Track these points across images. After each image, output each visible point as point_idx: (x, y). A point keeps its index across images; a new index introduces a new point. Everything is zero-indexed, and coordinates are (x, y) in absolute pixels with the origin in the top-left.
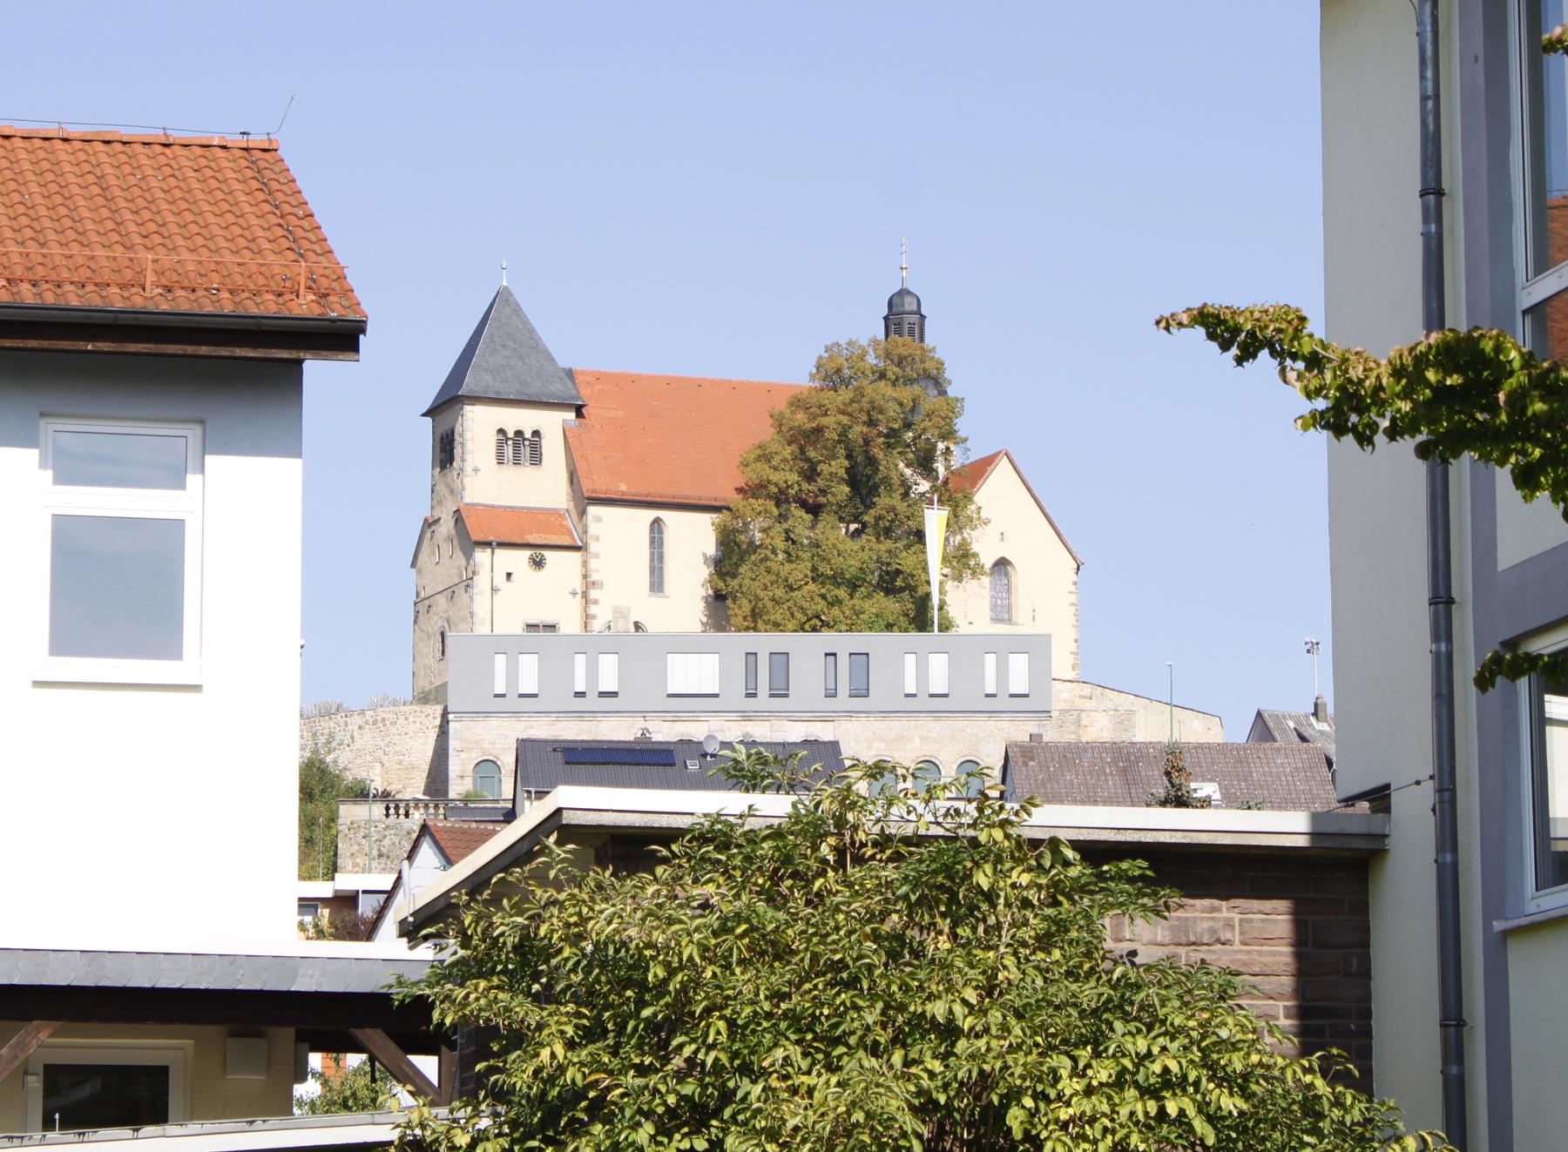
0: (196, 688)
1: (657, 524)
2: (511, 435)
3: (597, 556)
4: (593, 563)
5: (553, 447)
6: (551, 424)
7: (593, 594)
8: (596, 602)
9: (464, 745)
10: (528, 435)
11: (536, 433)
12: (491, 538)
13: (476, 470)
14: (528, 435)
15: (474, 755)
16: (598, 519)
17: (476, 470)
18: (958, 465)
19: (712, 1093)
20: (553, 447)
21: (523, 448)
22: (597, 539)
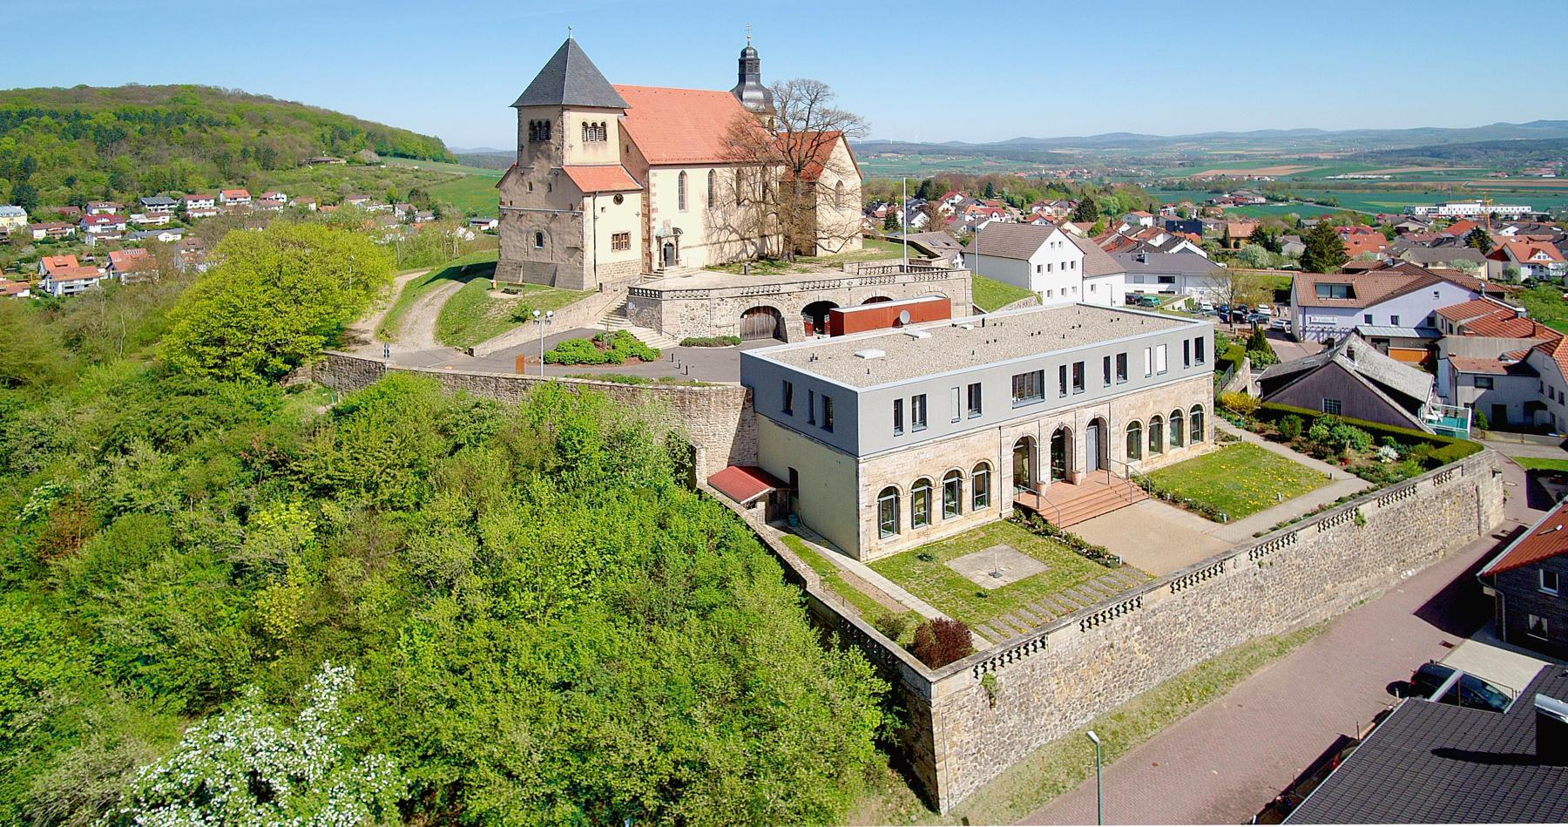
0: (1442, 752)
1: (682, 174)
2: (590, 125)
3: (655, 194)
4: (652, 199)
5: (612, 130)
6: (611, 120)
7: (653, 215)
8: (654, 220)
9: (871, 480)
10: (599, 125)
11: (603, 124)
12: (918, 329)
13: (571, 146)
14: (599, 125)
15: (879, 486)
16: (655, 175)
17: (571, 146)
18: (1495, 525)
19: (1539, 624)
20: (612, 130)
21: (596, 132)
22: (654, 185)
